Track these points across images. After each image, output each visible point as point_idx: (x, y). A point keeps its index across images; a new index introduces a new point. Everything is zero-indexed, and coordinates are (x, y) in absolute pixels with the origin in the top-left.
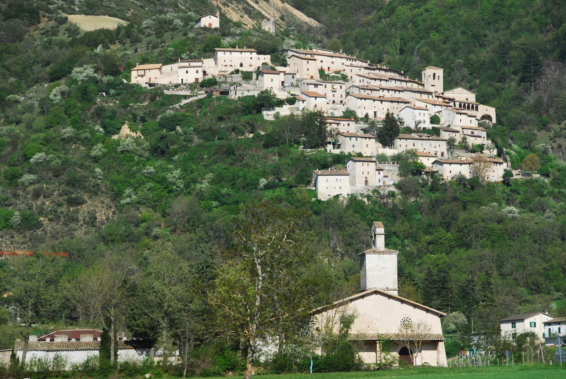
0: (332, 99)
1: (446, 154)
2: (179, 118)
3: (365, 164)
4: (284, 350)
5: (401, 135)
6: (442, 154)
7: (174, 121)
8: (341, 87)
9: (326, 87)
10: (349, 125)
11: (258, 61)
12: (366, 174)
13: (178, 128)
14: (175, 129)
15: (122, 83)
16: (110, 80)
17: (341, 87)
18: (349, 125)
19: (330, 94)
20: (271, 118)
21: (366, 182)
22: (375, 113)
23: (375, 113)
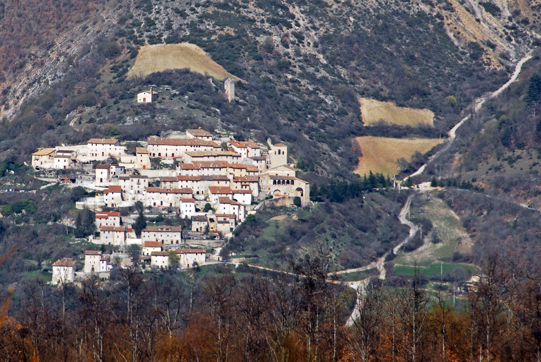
0: (137, 189)
1: (180, 242)
2: (23, 204)
3: (92, 256)
4: (504, 238)
5: (148, 228)
6: (177, 242)
7: (20, 206)
8: (145, 181)
9: (132, 180)
10: (115, 219)
11: (115, 151)
12: (92, 264)
13: (24, 211)
14: (21, 212)
15: (23, 165)
16: (335, 79)
17: (145, 181)
18: (115, 219)
19: (135, 186)
20: (80, 208)
21: (93, 269)
22: (162, 202)
23: (162, 202)
